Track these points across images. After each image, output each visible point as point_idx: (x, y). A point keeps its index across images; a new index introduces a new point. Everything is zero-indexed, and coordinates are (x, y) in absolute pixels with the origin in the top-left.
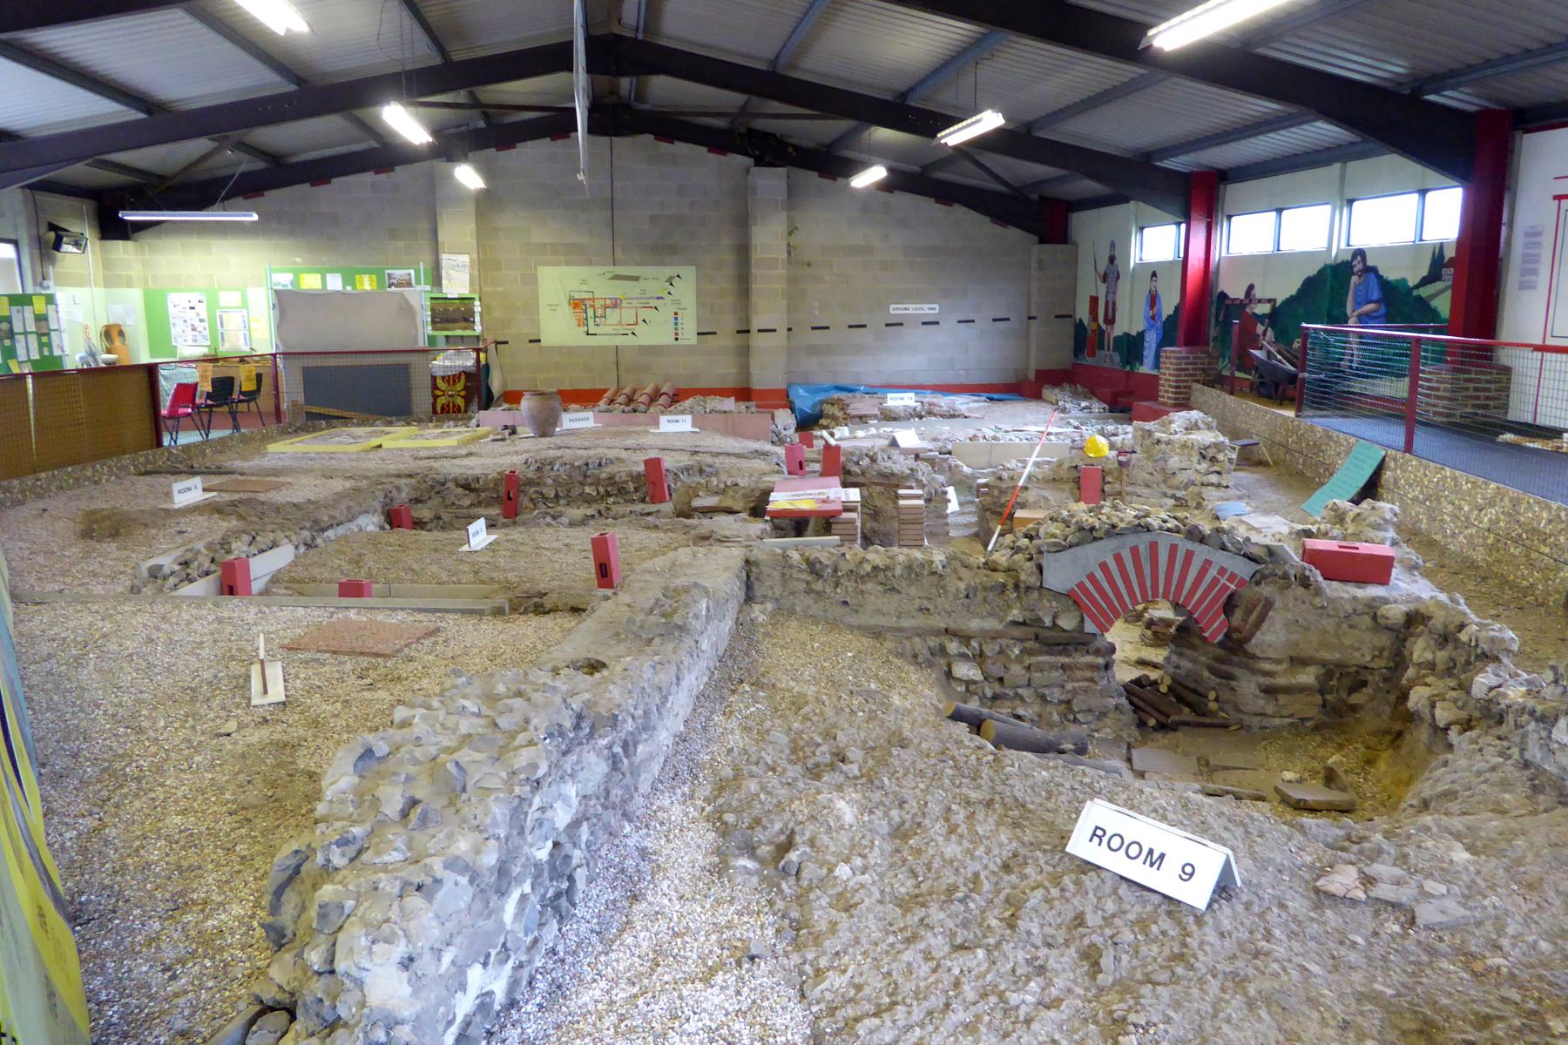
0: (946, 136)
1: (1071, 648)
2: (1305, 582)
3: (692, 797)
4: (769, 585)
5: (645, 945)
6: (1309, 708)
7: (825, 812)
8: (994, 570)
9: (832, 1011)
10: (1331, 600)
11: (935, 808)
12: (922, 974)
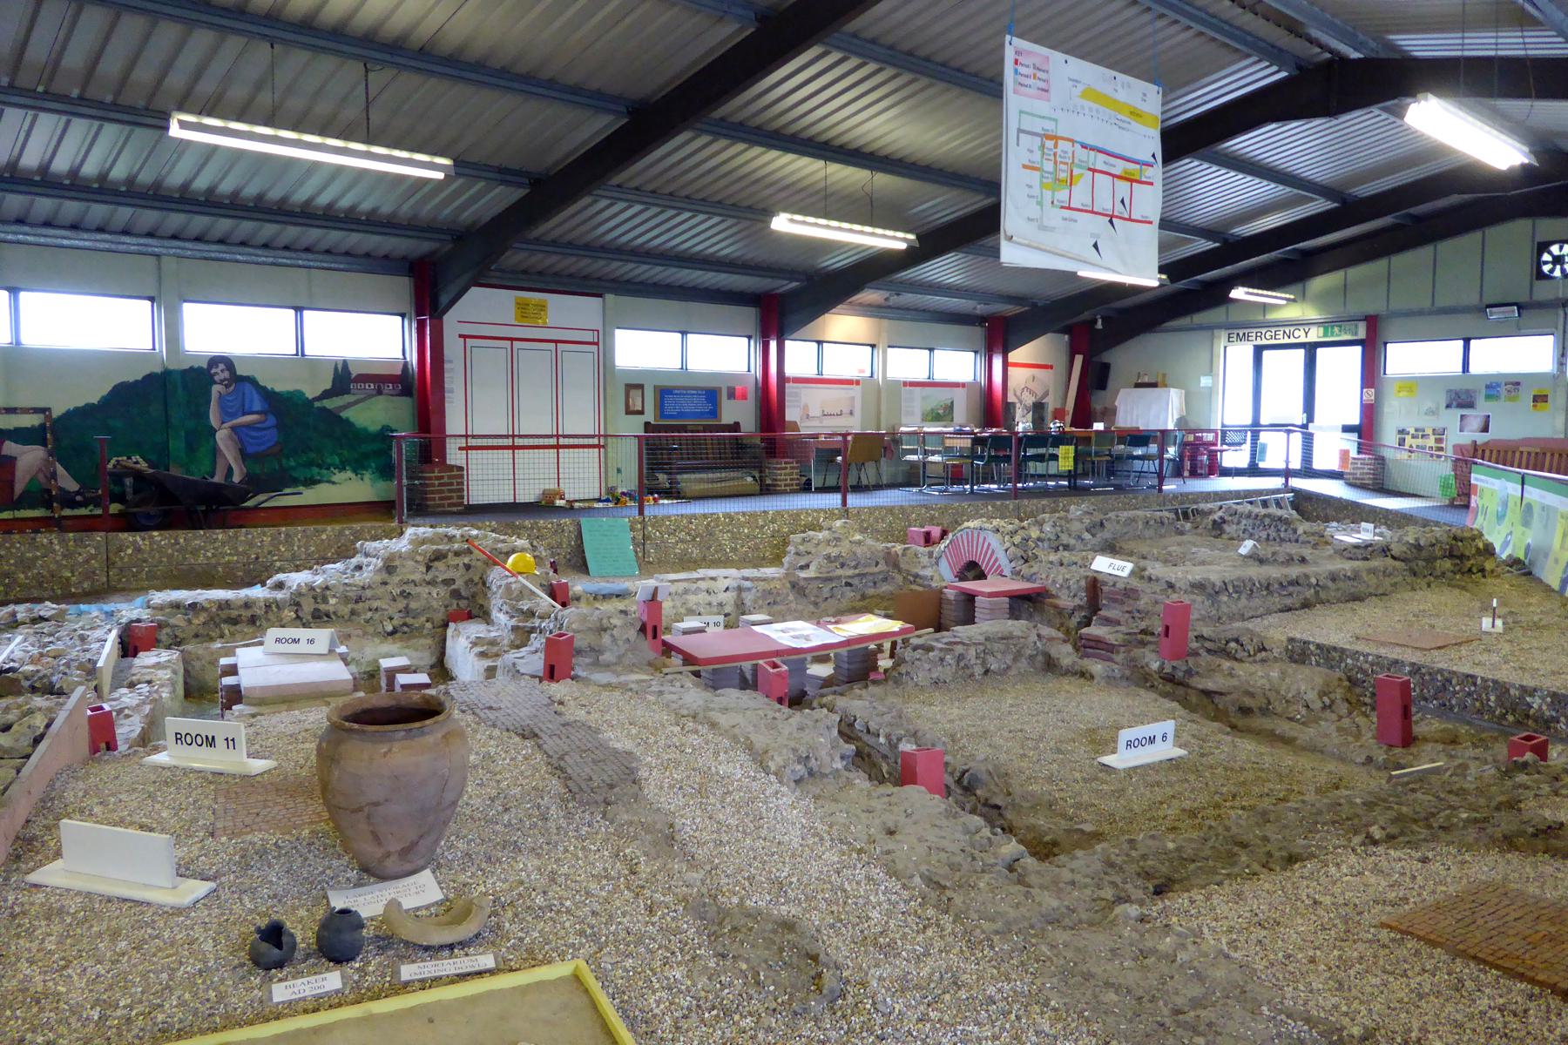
0: (606, 127)
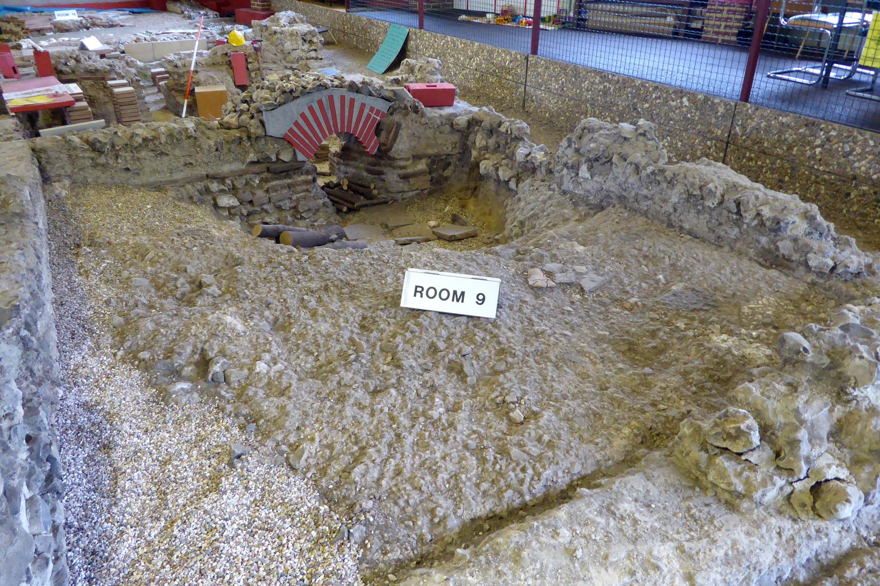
1: (291, 173)
2: (416, 110)
3: (99, 348)
4: (60, 165)
5: (142, 482)
6: (424, 183)
7: (220, 328)
8: (229, 128)
9: (323, 472)
10: (430, 119)
11: (293, 303)
12: (367, 421)
